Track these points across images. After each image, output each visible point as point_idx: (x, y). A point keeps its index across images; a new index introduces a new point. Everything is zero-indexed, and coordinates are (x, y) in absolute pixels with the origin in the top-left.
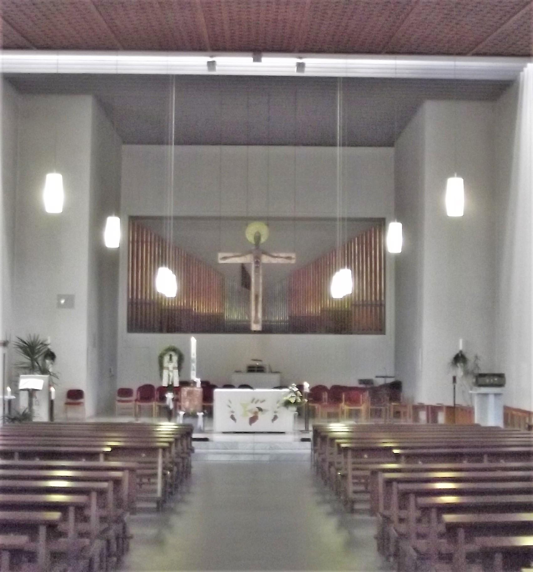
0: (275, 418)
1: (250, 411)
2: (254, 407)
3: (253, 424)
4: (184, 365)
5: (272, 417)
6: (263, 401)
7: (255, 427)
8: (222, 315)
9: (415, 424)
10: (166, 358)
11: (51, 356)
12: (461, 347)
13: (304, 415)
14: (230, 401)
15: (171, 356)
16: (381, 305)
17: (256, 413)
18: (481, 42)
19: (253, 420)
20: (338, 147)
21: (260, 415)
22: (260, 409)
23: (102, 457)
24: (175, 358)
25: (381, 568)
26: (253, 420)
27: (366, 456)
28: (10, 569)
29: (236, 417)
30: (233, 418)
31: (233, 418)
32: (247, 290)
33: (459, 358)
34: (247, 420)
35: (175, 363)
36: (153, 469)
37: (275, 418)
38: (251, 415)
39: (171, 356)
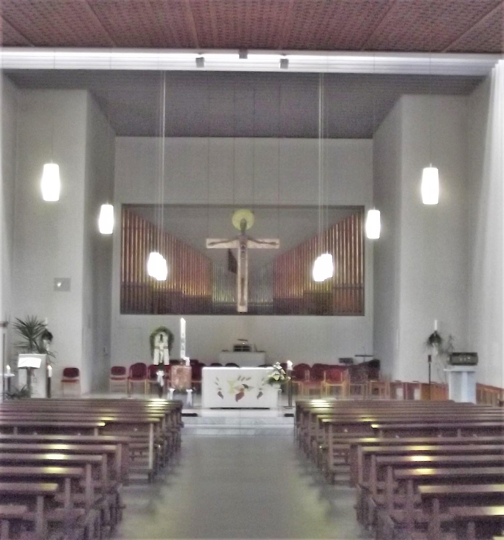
0: (260, 394)
1: (236, 388)
2: (240, 384)
3: (239, 401)
4: (174, 344)
5: (257, 394)
6: (249, 379)
7: (241, 403)
8: (210, 297)
9: (392, 400)
10: (157, 338)
11: (48, 336)
12: (436, 328)
13: (287, 391)
14: (217, 379)
15: (161, 336)
16: (361, 288)
17: (242, 390)
19: (239, 396)
20: (320, 139)
21: (246, 392)
22: (246, 387)
23: (96, 431)
24: (166, 338)
25: (360, 537)
26: (239, 396)
27: (346, 431)
28: (10, 537)
29: (223, 394)
30: (220, 394)
31: (220, 394)
32: (234, 274)
33: (434, 338)
34: (234, 397)
35: (165, 343)
36: (145, 442)
37: (260, 394)
38: (237, 392)
39: (161, 336)
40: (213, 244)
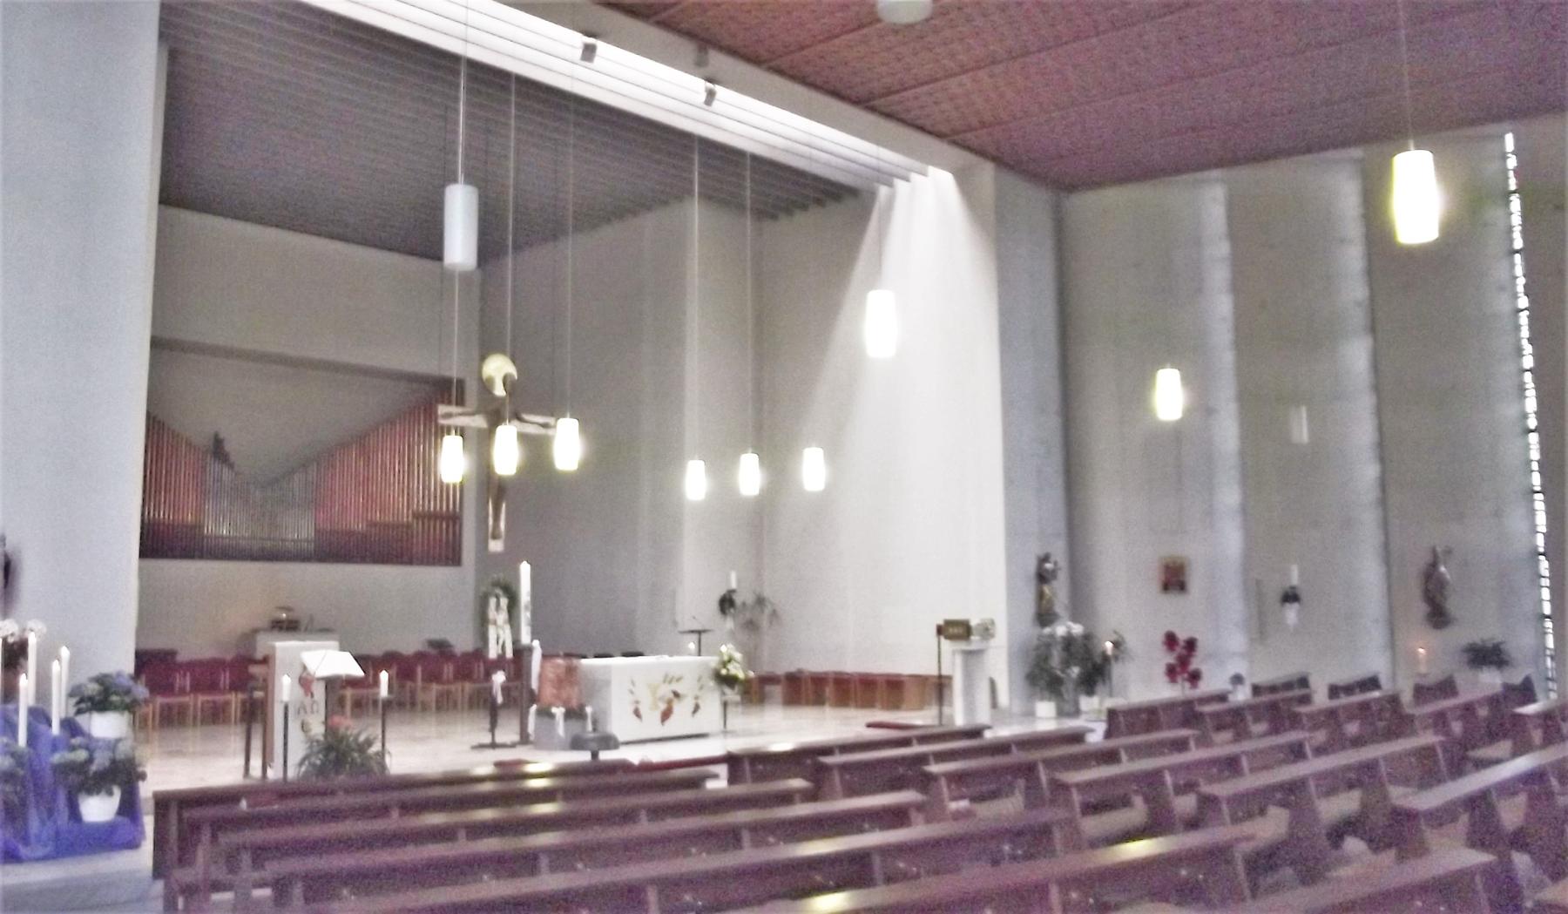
0: (697, 708)
1: (661, 699)
2: (666, 691)
3: (668, 723)
6: (678, 680)
7: (674, 726)
8: (198, 526)
9: (1386, 779)
10: (493, 601)
12: (734, 585)
14: (633, 683)
15: (498, 597)
18: (898, 92)
19: (666, 715)
22: (676, 695)
24: (504, 602)
25: (5, 640)
26: (666, 715)
28: (6, 902)
30: (637, 713)
31: (637, 713)
34: (658, 715)
36: (195, 718)
37: (697, 708)
38: (663, 706)
40: (449, 416)
